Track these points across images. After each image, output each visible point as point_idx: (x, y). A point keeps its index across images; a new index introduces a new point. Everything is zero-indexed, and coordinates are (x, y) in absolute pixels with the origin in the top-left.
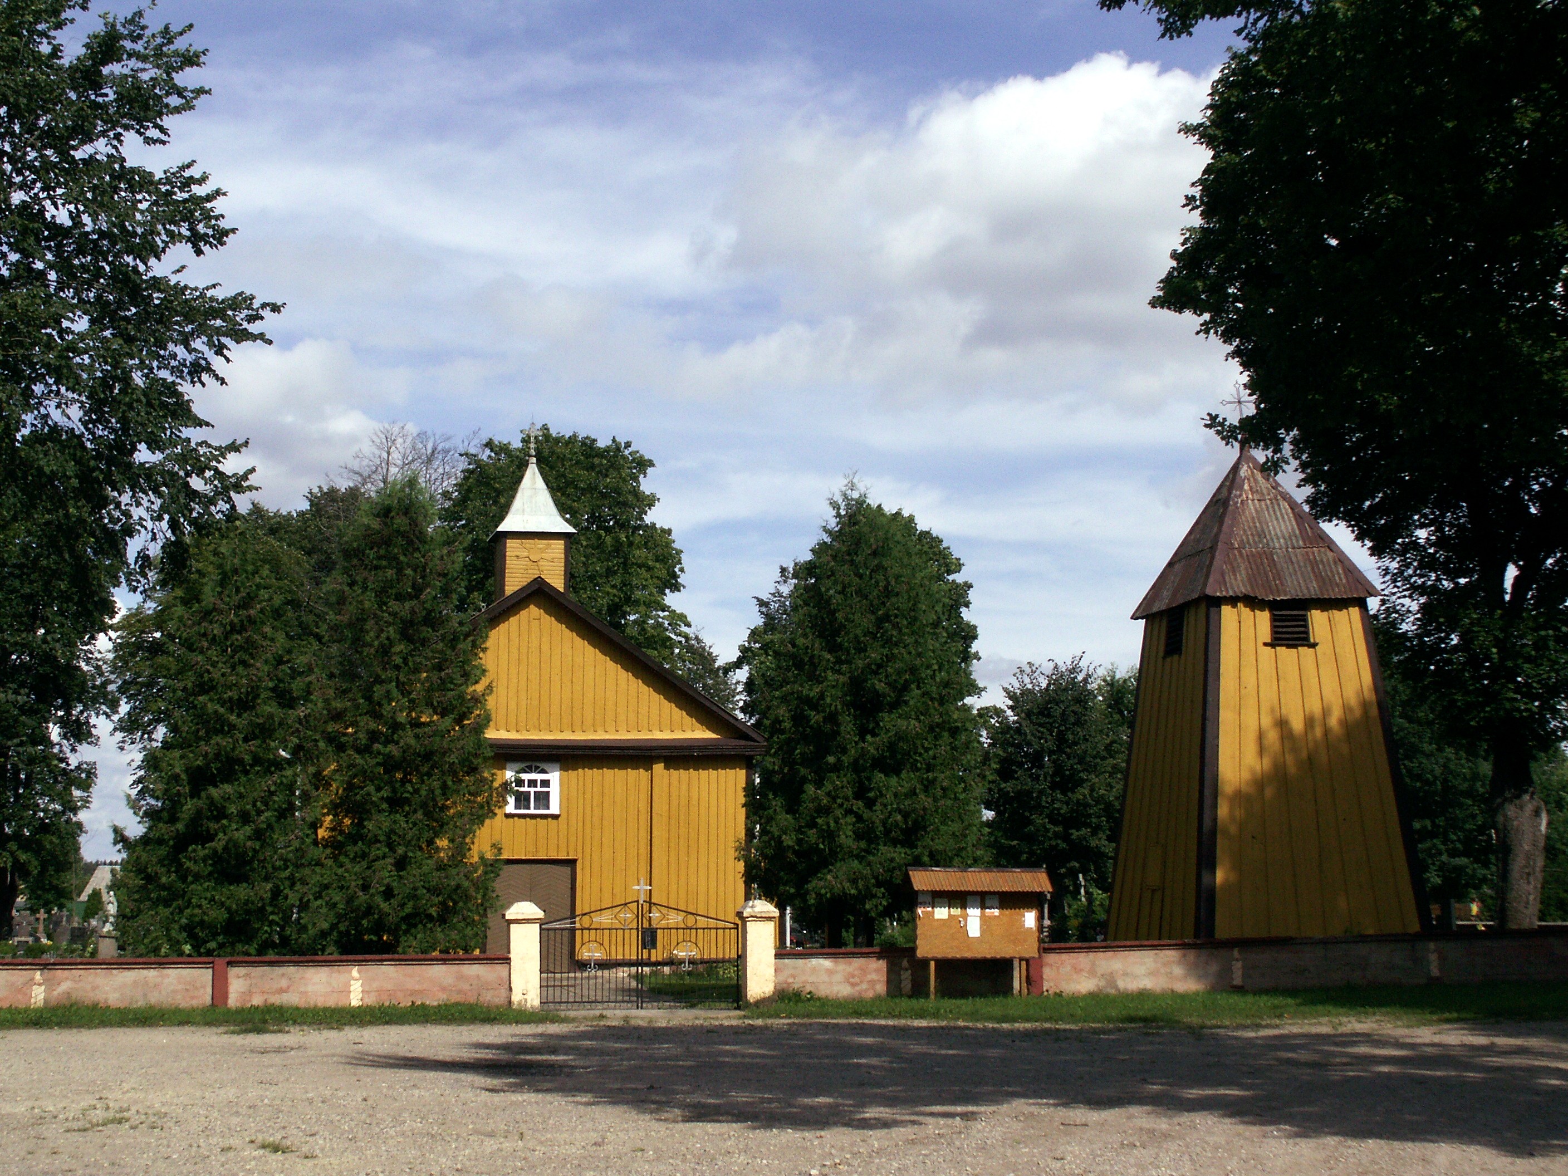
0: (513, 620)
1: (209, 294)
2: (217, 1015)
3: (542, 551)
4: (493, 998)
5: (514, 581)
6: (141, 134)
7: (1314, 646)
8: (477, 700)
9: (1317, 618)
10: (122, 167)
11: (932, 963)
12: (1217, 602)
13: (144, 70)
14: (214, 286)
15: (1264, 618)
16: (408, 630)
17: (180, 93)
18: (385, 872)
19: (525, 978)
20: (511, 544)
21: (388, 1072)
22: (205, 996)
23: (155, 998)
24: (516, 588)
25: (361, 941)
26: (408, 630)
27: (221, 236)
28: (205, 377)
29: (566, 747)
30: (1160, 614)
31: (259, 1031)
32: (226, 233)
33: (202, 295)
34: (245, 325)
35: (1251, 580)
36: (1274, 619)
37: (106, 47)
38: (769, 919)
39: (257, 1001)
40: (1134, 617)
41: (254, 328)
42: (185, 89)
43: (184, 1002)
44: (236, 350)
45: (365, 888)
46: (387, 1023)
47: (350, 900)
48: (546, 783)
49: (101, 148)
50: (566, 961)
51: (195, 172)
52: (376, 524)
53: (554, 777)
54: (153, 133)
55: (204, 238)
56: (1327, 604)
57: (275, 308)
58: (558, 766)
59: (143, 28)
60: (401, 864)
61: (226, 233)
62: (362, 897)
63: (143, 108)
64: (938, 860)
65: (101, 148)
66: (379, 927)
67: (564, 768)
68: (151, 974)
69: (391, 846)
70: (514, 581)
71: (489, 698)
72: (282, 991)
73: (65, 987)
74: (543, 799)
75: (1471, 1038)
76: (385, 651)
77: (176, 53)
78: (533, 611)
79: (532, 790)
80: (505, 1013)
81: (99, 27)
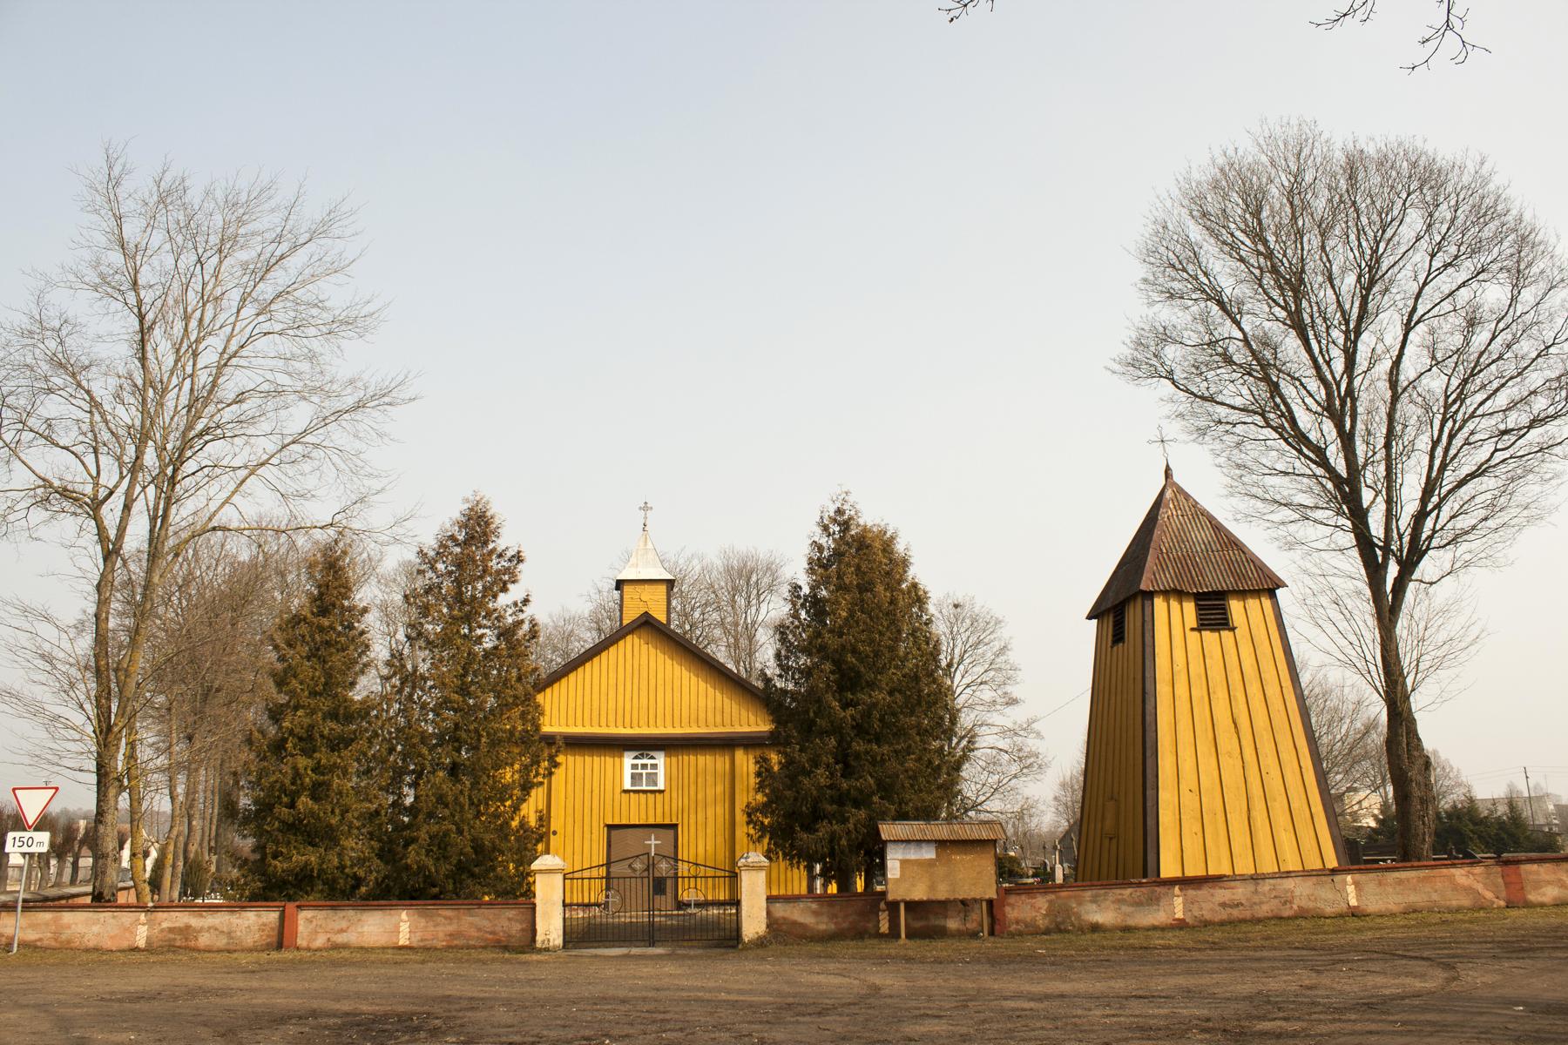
7: (1233, 629)
9: (1235, 606)
11: (902, 906)
12: (1150, 595)
15: (1190, 607)
22: (516, 928)
30: (1108, 611)
35: (1178, 576)
36: (1199, 608)
38: (761, 868)
40: (1090, 617)
48: (654, 766)
53: (660, 759)
56: (1243, 594)
64: (902, 816)
74: (652, 778)
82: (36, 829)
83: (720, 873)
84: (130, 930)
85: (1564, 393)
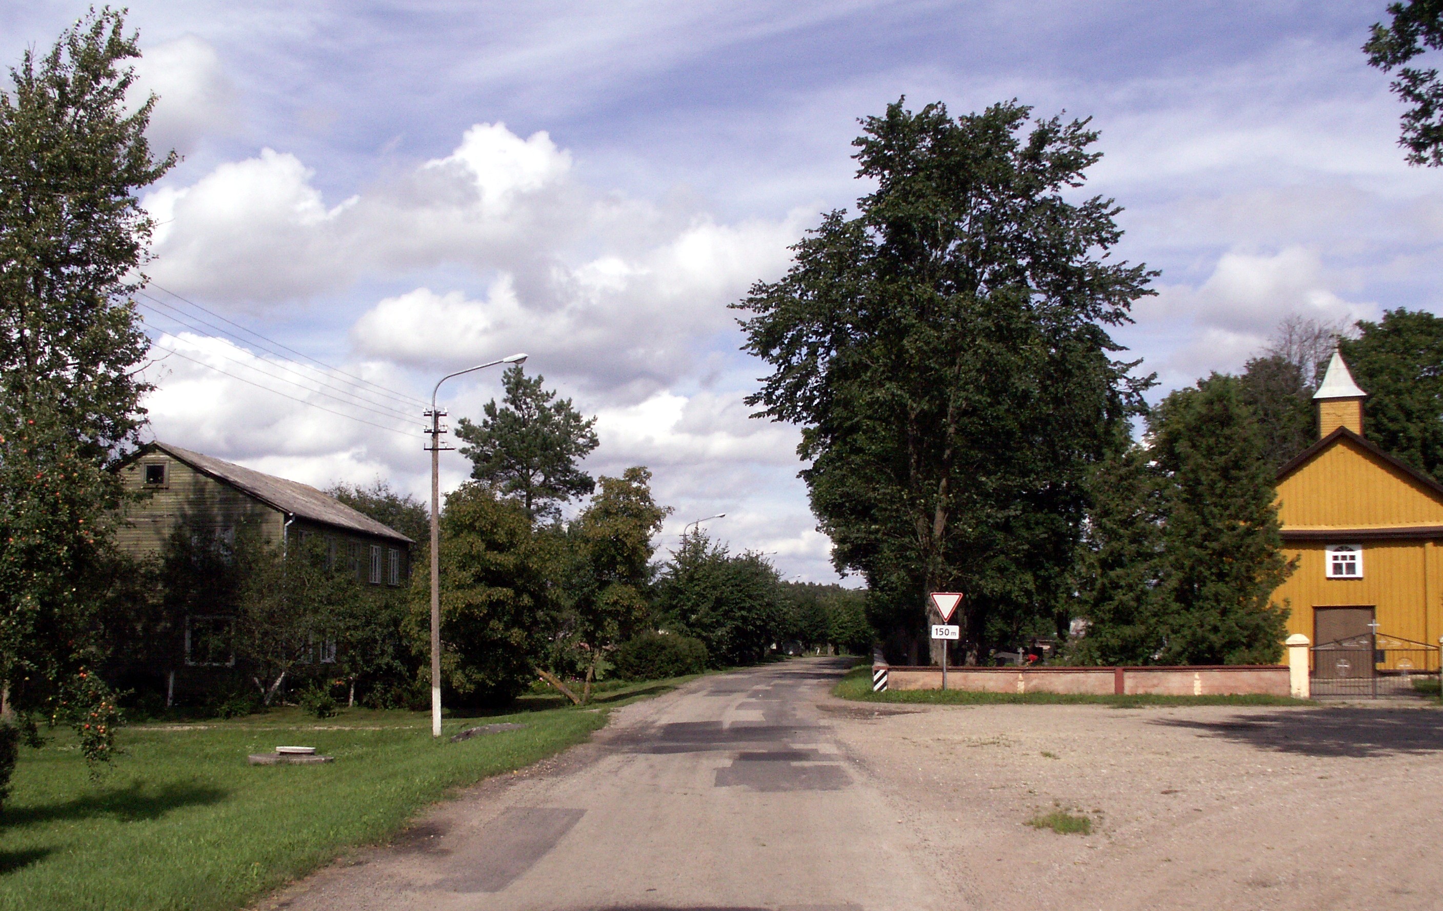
0: (1327, 454)
1: (1123, 267)
2: (1121, 700)
3: (1345, 408)
4: (1277, 691)
5: (1326, 430)
6: (1068, 182)
8: (1273, 512)
10: (1061, 203)
13: (1065, 147)
14: (1124, 263)
16: (1225, 473)
17: (1086, 157)
18: (1213, 618)
19: (1299, 680)
20: (1323, 406)
21: (1173, 728)
22: (1111, 689)
23: (1083, 689)
24: (1327, 434)
25: (1203, 656)
26: (1225, 473)
27: (1115, 238)
28: (1121, 320)
29: (1367, 534)
31: (1127, 707)
32: (1118, 235)
33: (1119, 270)
34: (1140, 287)
37: (1041, 138)
39: (1140, 691)
41: (1146, 287)
42: (1088, 155)
43: (1099, 692)
44: (1134, 303)
45: (1202, 626)
46: (1206, 704)
47: (1194, 634)
48: (1353, 558)
49: (1047, 192)
50: (1371, 671)
51: (1103, 201)
52: (1204, 411)
53: (1358, 553)
54: (1077, 179)
55: (1106, 239)
57: (1156, 274)
58: (1360, 546)
59: (1060, 126)
60: (1224, 612)
61: (1118, 235)
62: (1199, 631)
63: (1068, 165)
65: (1047, 192)
66: (1211, 648)
67: (1364, 548)
68: (1081, 676)
69: (1218, 601)
70: (1326, 430)
71: (1279, 511)
72: (1154, 686)
73: (1035, 682)
74: (1351, 568)
75: (1411, 702)
76: (1212, 486)
77: (1082, 136)
78: (1339, 449)
79: (1344, 562)
80: (1290, 701)
81: (1035, 128)
82: (949, 623)
83: (1414, 646)
84: (1013, 684)
85: (1441, 100)
